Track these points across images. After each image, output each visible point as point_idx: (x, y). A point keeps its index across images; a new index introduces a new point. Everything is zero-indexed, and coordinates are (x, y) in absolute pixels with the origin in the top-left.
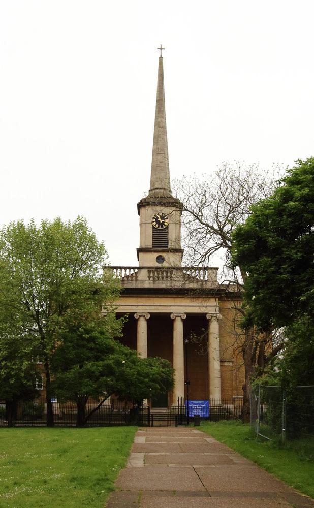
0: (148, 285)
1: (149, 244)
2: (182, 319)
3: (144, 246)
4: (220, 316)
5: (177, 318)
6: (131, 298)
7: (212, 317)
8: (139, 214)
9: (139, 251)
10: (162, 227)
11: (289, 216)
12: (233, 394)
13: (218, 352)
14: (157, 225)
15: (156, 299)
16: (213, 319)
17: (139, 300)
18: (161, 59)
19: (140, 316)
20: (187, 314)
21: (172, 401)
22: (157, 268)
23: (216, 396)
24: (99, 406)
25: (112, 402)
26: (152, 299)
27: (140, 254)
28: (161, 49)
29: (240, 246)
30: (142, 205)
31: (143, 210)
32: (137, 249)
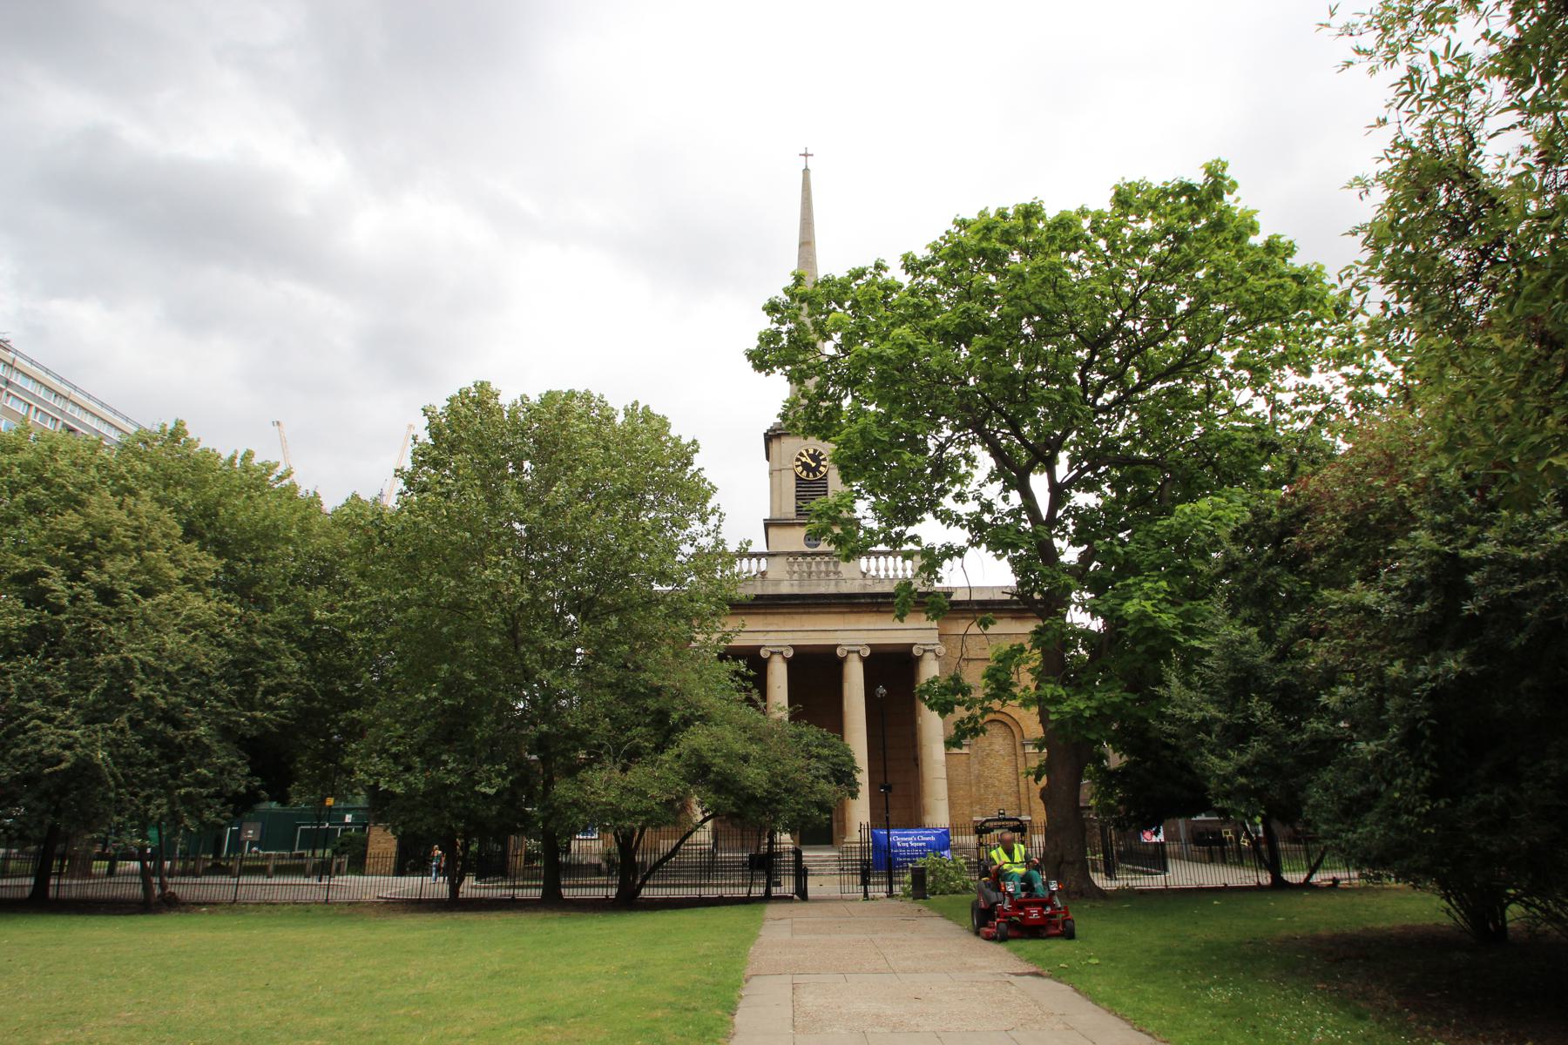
0: (785, 589)
1: (789, 510)
2: (861, 657)
3: (777, 516)
4: (941, 649)
5: (850, 655)
6: (754, 617)
7: (925, 651)
8: (768, 458)
9: (769, 525)
10: (815, 475)
11: (1509, 179)
12: (973, 813)
13: (944, 769)
14: (805, 473)
15: (805, 617)
16: (929, 656)
17: (770, 619)
18: (806, 171)
19: (772, 653)
20: (793, 647)
21: (843, 829)
22: (804, 555)
23: (939, 814)
24: (678, 846)
25: (716, 834)
26: (797, 617)
27: (772, 531)
28: (806, 155)
29: (1240, 333)
30: (771, 437)
31: (775, 445)
32: (355, 496)
